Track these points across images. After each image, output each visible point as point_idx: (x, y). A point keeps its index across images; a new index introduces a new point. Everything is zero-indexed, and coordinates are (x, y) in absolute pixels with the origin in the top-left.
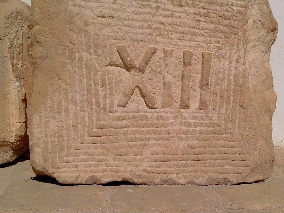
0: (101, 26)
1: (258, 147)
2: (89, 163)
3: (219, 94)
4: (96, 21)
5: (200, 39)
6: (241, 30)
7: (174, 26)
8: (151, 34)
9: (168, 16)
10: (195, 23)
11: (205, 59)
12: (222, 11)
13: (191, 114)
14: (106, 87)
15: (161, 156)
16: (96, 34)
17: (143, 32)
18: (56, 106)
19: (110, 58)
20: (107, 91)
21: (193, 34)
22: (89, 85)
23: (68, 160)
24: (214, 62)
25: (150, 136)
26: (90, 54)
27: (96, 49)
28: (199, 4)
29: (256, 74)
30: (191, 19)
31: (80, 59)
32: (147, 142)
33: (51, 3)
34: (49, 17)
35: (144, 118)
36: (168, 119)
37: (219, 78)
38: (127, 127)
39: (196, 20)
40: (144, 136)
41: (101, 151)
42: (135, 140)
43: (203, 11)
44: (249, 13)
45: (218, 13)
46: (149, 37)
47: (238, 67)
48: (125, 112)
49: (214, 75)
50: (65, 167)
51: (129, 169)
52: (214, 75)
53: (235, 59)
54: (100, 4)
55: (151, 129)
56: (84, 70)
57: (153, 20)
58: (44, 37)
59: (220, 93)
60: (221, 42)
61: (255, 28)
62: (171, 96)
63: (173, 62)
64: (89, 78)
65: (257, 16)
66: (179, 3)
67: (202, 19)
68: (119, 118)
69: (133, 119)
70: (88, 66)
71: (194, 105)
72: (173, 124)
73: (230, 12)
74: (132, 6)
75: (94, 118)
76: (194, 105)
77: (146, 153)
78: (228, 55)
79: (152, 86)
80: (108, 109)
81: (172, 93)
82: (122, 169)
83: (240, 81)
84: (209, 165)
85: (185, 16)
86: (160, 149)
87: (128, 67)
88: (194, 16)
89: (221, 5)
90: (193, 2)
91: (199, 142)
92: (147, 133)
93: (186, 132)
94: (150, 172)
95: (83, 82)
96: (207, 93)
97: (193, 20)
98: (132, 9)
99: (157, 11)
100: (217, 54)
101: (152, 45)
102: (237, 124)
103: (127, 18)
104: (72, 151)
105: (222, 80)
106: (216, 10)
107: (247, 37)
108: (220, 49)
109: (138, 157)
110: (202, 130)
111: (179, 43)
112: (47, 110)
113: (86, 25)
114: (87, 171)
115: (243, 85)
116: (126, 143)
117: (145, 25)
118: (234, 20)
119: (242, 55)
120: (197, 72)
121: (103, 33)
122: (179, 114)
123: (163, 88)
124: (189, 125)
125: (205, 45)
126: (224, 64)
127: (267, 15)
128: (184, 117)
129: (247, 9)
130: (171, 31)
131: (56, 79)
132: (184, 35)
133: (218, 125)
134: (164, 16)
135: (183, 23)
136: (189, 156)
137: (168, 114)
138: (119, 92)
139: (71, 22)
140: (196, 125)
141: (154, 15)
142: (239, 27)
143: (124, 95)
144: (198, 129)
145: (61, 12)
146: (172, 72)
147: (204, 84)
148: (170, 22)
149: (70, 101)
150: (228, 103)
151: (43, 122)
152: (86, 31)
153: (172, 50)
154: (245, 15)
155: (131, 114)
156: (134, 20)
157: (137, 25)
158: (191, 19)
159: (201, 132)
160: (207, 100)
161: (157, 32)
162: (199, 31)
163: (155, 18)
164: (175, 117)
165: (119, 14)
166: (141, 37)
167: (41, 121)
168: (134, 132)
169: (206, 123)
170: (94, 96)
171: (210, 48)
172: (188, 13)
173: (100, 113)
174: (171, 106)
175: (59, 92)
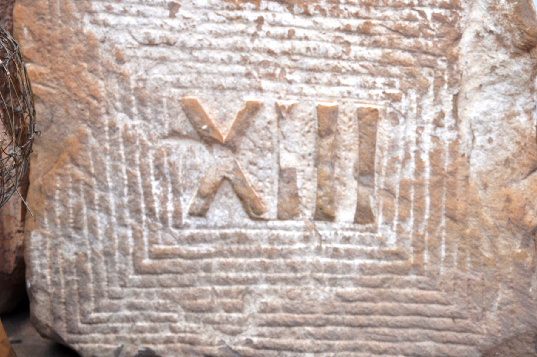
0: (149, 62)
1: (497, 304)
2: (139, 324)
3: (397, 191)
4: (140, 53)
5: (352, 80)
6: (444, 58)
7: (295, 57)
8: (248, 75)
9: (282, 38)
10: (340, 49)
11: (367, 120)
12: (397, 20)
13: (339, 232)
14: (165, 179)
15: (281, 316)
16: (140, 79)
17: (232, 72)
18: (71, 216)
19: (170, 124)
20: (167, 187)
21: (336, 70)
22: (131, 176)
23: (98, 318)
24: (384, 127)
25: (257, 274)
26: (131, 117)
27: (141, 108)
28: (346, 9)
29: (489, 146)
30: (330, 40)
31: (113, 128)
32: (252, 287)
33: (51, 21)
34: (49, 48)
35: (242, 239)
36: (292, 242)
37: (395, 160)
38: (209, 255)
39: (341, 43)
40: (244, 275)
41: (161, 301)
42: (226, 281)
43: (355, 23)
44: (463, 19)
45: (390, 24)
46: (245, 81)
47: (438, 135)
48: (205, 227)
49: (385, 153)
50: (93, 331)
51: (217, 339)
52: (385, 153)
53: (431, 120)
54: (145, 21)
55: (258, 260)
56: (122, 147)
57: (251, 46)
58: (44, 85)
59: (400, 189)
60: (397, 83)
61: (479, 49)
62: (295, 196)
63: (297, 129)
64: (131, 162)
65: (483, 22)
66: (302, 10)
67: (354, 39)
68: (192, 240)
69: (222, 241)
70: (128, 140)
71: (346, 215)
72: (302, 252)
73: (416, 20)
74: (208, 21)
75: (145, 239)
76: (346, 215)
77: (252, 308)
78: (415, 111)
79: (255, 175)
80: (170, 221)
81: (297, 189)
82: (204, 338)
83: (446, 164)
84: (384, 337)
85: (317, 36)
86: (277, 302)
87: (210, 140)
88: (337, 34)
89: (396, 7)
90: (334, 5)
91: (360, 288)
92: (251, 269)
93: (330, 269)
94: (260, 346)
95: (121, 171)
96: (372, 190)
97: (334, 42)
98: (209, 27)
99: (259, 28)
100: (389, 110)
101: (252, 97)
102: (443, 254)
103: (199, 46)
104: (105, 301)
105: (404, 164)
106: (385, 18)
107: (458, 72)
108: (396, 99)
109: (235, 315)
110: (365, 265)
111: (307, 89)
112: (56, 225)
113: (120, 60)
114: (136, 340)
115: (452, 173)
116: (209, 288)
117: (237, 57)
118: (426, 36)
119: (448, 108)
120: (348, 148)
121: (153, 77)
122: (313, 232)
123: (279, 181)
124: (336, 253)
125: (363, 93)
126: (408, 130)
127: (510, 18)
128: (323, 238)
129: (458, 12)
130: (289, 67)
131: (69, 166)
132: (318, 75)
133: (398, 255)
134: (276, 37)
135: (315, 49)
136: (339, 318)
137: (292, 229)
138: (192, 188)
139: (91, 57)
140: (349, 254)
141: (254, 36)
142: (437, 52)
143: (201, 195)
144: (357, 262)
145: (71, 37)
146: (297, 149)
147: (365, 172)
148: (287, 50)
149: (97, 207)
150: (420, 210)
151: (48, 246)
152: (121, 74)
153: (293, 105)
154: (451, 24)
155: (217, 232)
156: (215, 49)
157: (220, 59)
158: (330, 40)
159: (362, 269)
160: (372, 205)
161: (262, 70)
162: (349, 63)
163: (256, 42)
164: (306, 239)
165: (183, 37)
166: (228, 81)
167: (44, 244)
168: (224, 267)
169: (373, 251)
170: (142, 197)
171: (375, 97)
172: (323, 29)
173: (155, 229)
174: (296, 215)
175: (76, 190)
